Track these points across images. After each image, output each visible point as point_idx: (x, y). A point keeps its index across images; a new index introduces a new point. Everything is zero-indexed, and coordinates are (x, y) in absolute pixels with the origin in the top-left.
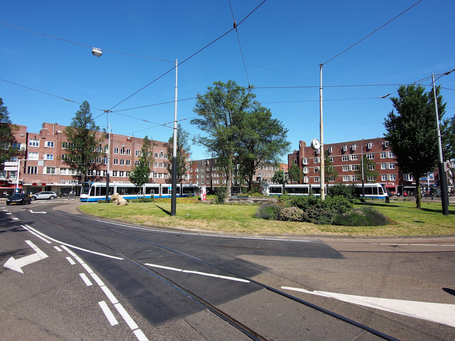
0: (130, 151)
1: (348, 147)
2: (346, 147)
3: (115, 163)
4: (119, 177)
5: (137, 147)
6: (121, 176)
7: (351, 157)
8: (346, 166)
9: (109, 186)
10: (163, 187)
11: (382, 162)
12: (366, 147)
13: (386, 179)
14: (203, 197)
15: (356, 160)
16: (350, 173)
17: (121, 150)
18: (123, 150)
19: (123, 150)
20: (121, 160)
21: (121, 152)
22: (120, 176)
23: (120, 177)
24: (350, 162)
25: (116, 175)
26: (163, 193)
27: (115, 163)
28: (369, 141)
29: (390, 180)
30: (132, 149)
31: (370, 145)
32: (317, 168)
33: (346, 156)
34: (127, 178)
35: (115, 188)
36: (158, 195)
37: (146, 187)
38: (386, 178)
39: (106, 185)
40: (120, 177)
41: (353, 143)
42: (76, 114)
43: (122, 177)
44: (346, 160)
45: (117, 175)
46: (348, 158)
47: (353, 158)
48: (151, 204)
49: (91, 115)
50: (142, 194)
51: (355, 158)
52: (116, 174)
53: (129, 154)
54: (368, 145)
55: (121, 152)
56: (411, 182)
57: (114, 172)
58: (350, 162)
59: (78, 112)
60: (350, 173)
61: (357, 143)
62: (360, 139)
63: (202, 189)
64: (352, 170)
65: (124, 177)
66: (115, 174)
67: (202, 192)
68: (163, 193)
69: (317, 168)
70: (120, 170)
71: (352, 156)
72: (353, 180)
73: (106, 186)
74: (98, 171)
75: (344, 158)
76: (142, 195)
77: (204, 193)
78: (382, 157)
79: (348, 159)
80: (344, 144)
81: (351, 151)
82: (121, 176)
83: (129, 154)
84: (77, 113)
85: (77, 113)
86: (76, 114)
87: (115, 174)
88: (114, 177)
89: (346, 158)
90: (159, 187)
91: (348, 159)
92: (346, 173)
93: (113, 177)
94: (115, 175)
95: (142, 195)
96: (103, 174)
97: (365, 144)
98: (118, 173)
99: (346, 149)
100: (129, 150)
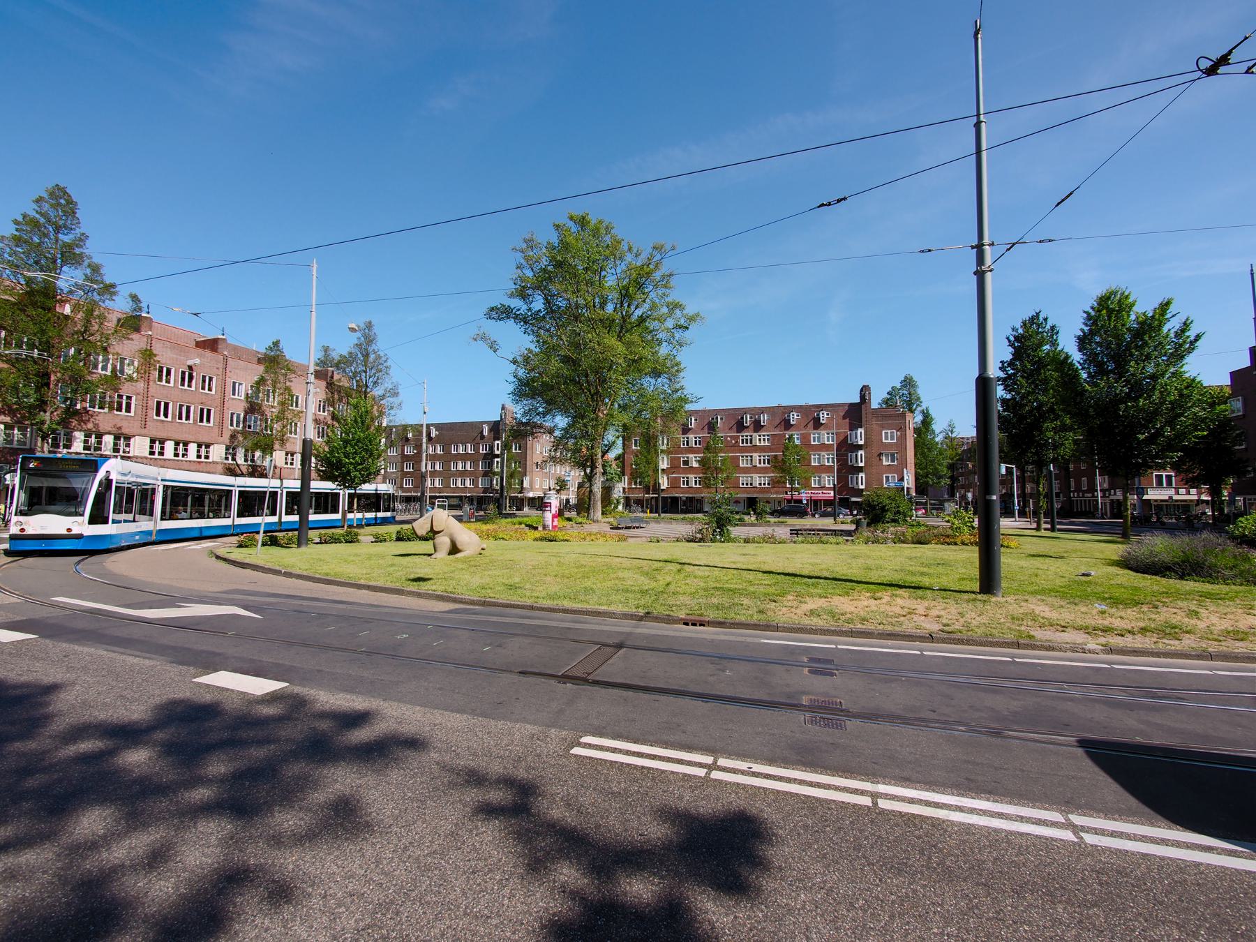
0: (214, 380)
1: (751, 418)
2: (693, 419)
3: (158, 414)
4: (174, 460)
5: (236, 371)
6: (181, 455)
7: (758, 437)
8: (747, 456)
9: (311, 491)
10: (287, 492)
11: (813, 451)
12: (814, 418)
13: (819, 483)
14: (553, 521)
15: (767, 444)
16: (754, 469)
17: (183, 373)
18: (187, 374)
19: (187, 374)
20: (181, 406)
21: (183, 379)
22: (176, 455)
23: (178, 461)
24: (756, 449)
25: (161, 454)
26: (286, 514)
27: (158, 414)
28: (791, 409)
29: (827, 486)
30: (220, 374)
31: (794, 418)
32: (688, 458)
33: (747, 436)
34: (199, 462)
35: (282, 494)
36: (338, 516)
37: (239, 491)
38: (819, 481)
39: (299, 486)
40: (176, 458)
41: (762, 410)
42: (16, 222)
43: (182, 461)
44: (747, 443)
45: (166, 451)
46: (751, 440)
47: (760, 440)
48: (1080, 551)
49: (83, 239)
50: (273, 513)
51: (764, 440)
52: (162, 448)
53: (210, 389)
54: (789, 416)
55: (183, 379)
56: (862, 490)
57: (153, 441)
58: (756, 449)
59: (25, 216)
60: (754, 469)
61: (770, 410)
62: (803, 403)
63: (549, 498)
64: (758, 465)
65: (190, 461)
66: (203, 454)
67: (549, 508)
68: (286, 514)
69: (688, 458)
70: (200, 440)
71: (760, 436)
72: (760, 484)
73: (299, 490)
74: (122, 439)
75: (743, 440)
76: (275, 519)
77: (554, 512)
78: (814, 441)
79: (751, 443)
80: (745, 411)
81: (758, 426)
82: (181, 455)
83: (210, 389)
84: (20, 219)
85: (20, 219)
86: (16, 222)
87: (203, 454)
88: (156, 459)
89: (747, 440)
90: (277, 492)
91: (751, 443)
92: (746, 471)
93: (151, 459)
94: (203, 457)
95: (275, 519)
96: (148, 450)
97: (785, 413)
98: (193, 448)
99: (748, 420)
100: (211, 379)
